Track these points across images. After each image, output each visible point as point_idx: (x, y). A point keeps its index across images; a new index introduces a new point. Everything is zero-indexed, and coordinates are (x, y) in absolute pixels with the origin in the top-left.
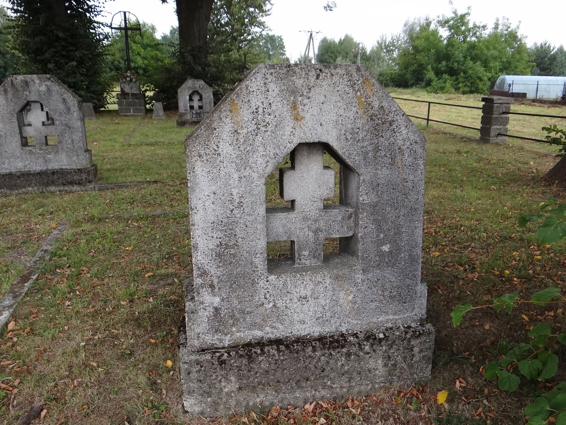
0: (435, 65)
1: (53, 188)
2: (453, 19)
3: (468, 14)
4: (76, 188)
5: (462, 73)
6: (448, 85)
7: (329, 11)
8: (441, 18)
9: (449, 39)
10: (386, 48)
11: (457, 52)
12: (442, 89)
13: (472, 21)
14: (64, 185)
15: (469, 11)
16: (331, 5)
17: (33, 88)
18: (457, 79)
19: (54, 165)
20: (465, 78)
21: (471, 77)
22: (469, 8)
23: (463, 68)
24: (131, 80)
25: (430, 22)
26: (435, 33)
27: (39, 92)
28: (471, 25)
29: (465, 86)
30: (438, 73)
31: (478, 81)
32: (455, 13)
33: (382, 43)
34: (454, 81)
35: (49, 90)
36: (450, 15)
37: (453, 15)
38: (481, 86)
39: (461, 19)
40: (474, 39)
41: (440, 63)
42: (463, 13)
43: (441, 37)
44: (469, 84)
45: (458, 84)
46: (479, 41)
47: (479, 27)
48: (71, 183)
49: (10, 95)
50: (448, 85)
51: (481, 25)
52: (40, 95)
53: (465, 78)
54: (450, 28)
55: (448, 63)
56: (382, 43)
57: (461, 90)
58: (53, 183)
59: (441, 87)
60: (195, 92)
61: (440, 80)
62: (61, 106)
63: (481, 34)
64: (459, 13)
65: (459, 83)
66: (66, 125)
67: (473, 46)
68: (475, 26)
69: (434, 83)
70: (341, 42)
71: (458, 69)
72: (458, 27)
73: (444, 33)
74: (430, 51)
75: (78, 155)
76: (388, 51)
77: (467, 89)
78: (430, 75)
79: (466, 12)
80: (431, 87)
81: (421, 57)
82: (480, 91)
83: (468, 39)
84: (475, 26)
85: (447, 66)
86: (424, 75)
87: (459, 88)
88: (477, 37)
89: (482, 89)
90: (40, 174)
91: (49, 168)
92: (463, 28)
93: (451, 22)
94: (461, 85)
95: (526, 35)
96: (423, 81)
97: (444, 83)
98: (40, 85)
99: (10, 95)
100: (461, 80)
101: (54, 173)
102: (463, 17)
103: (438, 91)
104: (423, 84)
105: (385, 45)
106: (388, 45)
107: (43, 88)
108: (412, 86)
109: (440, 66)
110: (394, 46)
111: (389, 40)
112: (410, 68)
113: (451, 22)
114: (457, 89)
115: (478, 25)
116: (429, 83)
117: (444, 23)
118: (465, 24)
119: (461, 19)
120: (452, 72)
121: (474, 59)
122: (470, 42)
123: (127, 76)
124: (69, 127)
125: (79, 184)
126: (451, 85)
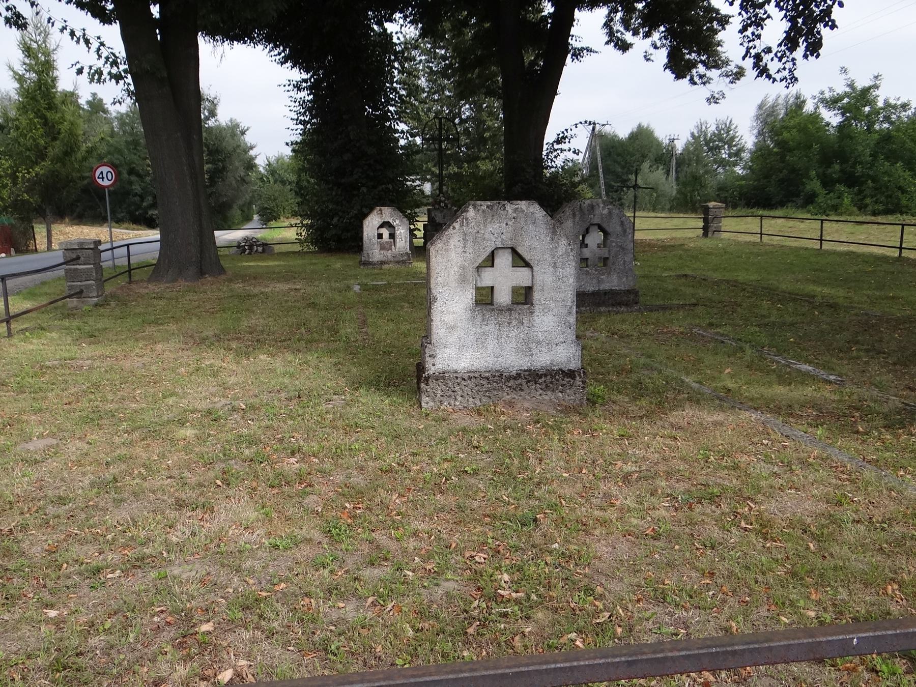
0: (821, 170)
1: (603, 309)
2: (846, 95)
3: (876, 87)
4: (623, 309)
5: (870, 182)
6: (847, 201)
7: (713, 104)
8: (827, 95)
9: (841, 127)
10: (707, 144)
11: (860, 148)
12: (835, 209)
13: (882, 96)
14: (613, 305)
15: (878, 82)
16: (717, 96)
17: (597, 212)
18: (860, 192)
19: (606, 286)
20: (876, 189)
21: (887, 187)
22: (876, 77)
23: (871, 173)
24: (446, 206)
25: (804, 102)
26: (815, 118)
27: (602, 215)
28: (880, 104)
29: (876, 202)
30: (828, 183)
31: (899, 193)
32: (851, 86)
33: (699, 137)
34: (857, 194)
35: (610, 213)
36: (841, 88)
37: (848, 90)
38: (904, 202)
39: (864, 96)
40: (886, 125)
41: (829, 166)
42: (867, 85)
43: (828, 124)
44: (883, 199)
45: (862, 200)
46: (898, 130)
47: (895, 107)
48: (620, 304)
49: (577, 218)
50: (847, 201)
51: (899, 103)
52: (602, 219)
53: (876, 189)
54: (844, 110)
55: (844, 166)
56: (699, 137)
57: (870, 208)
58: (603, 304)
59: (833, 206)
60: (385, 224)
61: (832, 194)
62: (619, 229)
63: (899, 117)
64: (859, 85)
65: (865, 197)
66: (621, 246)
67: (886, 138)
68: (887, 105)
69: (820, 199)
70: (634, 137)
71: (862, 176)
72: (858, 109)
73: (832, 118)
74: (811, 147)
75: (627, 277)
76: (710, 149)
77: (881, 207)
78: (815, 185)
79: (872, 83)
80: (815, 205)
81: (795, 158)
82: (904, 210)
83: (877, 127)
84: (887, 105)
85: (842, 171)
86: (801, 188)
87: (866, 206)
88: (891, 123)
89: (907, 206)
90: (594, 294)
91: (601, 288)
92: (867, 109)
93: (846, 100)
94: (868, 201)
95: (903, 100)
96: (798, 196)
97: (839, 198)
98: (603, 208)
99: (577, 218)
100: (868, 192)
101: (606, 293)
102: (866, 91)
103: (828, 212)
104: (800, 202)
105: (705, 139)
106: (711, 139)
107: (606, 212)
108: (781, 204)
109: (830, 171)
110: (721, 140)
111: (712, 129)
112: (774, 177)
113: (846, 100)
114: (862, 208)
115: (892, 102)
116: (809, 200)
117: (832, 103)
118: (872, 103)
119: (679, 67)
120: (851, 181)
121: (893, 157)
122: (881, 130)
123: (441, 201)
124: (623, 249)
125: (627, 305)
126: (852, 201)
